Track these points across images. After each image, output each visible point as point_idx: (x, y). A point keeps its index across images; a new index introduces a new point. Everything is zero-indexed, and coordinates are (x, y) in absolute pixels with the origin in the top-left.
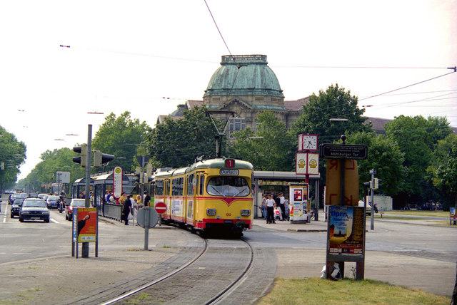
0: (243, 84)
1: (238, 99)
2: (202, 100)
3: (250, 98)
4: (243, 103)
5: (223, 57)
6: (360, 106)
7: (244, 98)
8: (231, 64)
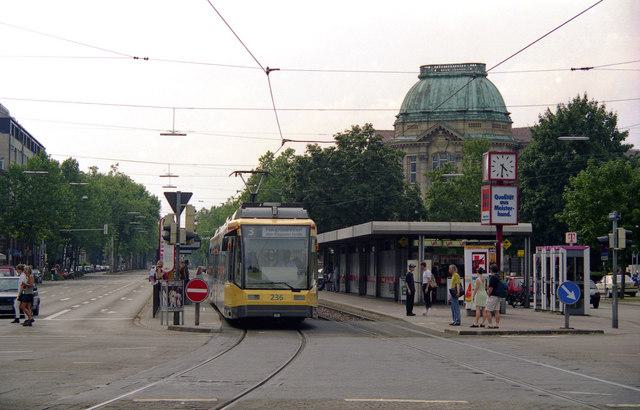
0: (452, 103)
1: (443, 127)
2: (393, 129)
3: (461, 126)
4: (451, 131)
5: (422, 68)
6: (620, 127)
7: (453, 125)
8: (434, 77)
